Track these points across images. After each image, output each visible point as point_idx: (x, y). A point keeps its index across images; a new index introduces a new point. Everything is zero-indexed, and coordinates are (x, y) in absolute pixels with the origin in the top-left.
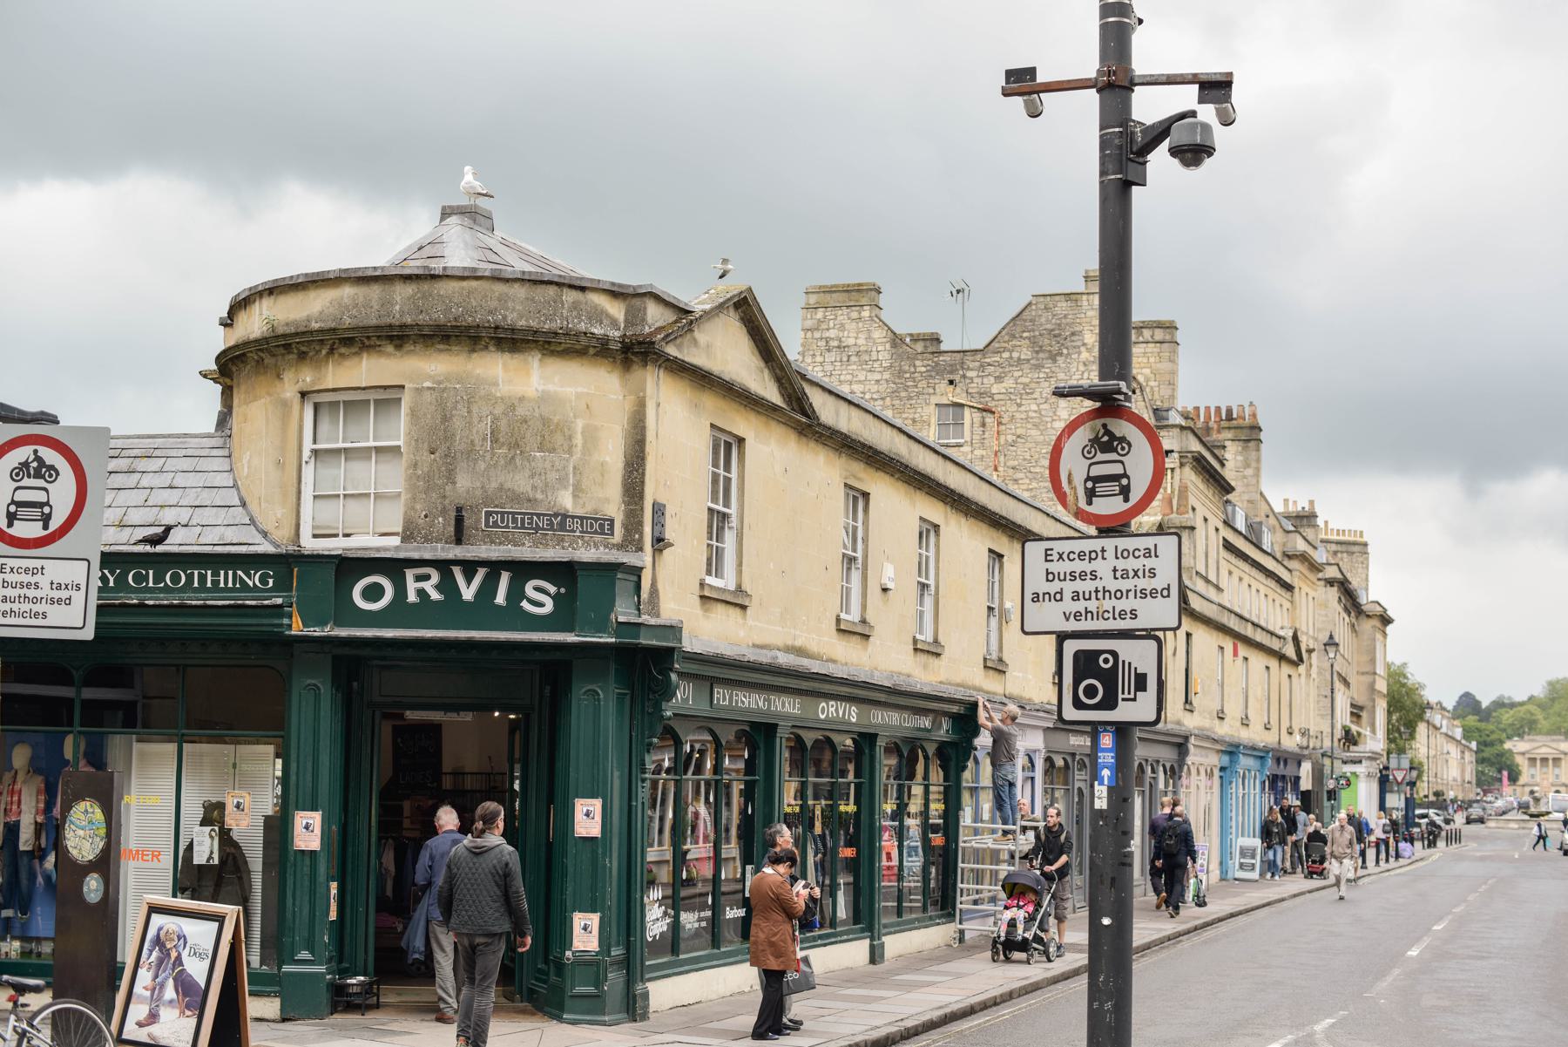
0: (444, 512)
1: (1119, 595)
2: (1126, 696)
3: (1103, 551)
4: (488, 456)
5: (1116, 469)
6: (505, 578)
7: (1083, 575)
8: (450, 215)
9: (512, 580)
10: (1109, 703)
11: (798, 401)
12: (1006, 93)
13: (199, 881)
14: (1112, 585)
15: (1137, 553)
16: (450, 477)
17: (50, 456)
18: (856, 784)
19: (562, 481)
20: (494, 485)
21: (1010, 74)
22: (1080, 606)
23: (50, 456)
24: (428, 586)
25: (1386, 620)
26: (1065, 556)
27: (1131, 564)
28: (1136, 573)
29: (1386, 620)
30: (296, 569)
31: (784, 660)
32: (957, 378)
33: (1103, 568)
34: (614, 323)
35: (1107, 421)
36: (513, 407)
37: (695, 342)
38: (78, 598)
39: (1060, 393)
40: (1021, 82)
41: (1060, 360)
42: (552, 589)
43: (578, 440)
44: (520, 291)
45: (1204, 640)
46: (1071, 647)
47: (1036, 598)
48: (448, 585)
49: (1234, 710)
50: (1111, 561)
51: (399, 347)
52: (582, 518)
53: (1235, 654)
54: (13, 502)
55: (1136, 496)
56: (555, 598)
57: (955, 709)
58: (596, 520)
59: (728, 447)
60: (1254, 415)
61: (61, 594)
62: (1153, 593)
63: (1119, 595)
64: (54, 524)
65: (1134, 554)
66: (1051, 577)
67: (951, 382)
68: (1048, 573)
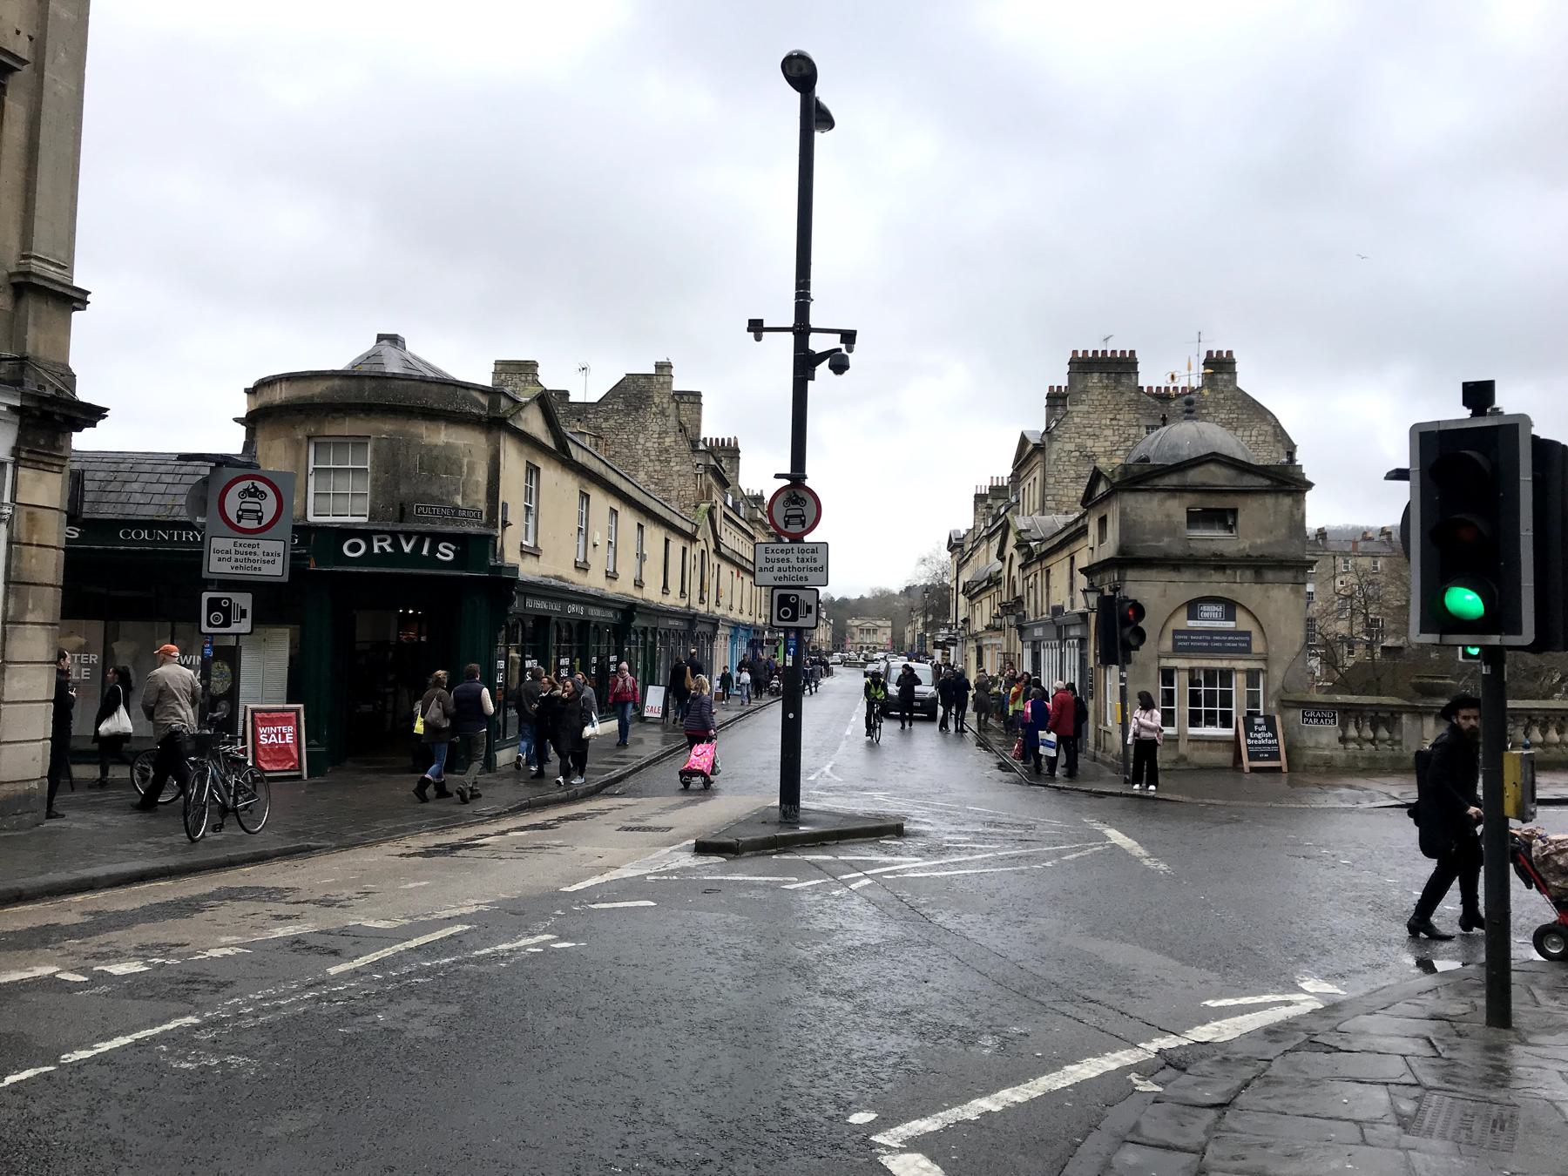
0: (393, 506)
1: (799, 569)
7: (783, 560)
8: (382, 340)
10: (795, 618)
12: (749, 330)
13: (1527, 737)
14: (797, 565)
16: (397, 487)
17: (261, 486)
18: (578, 647)
21: (750, 321)
23: (261, 486)
24: (385, 545)
27: (806, 556)
30: (313, 536)
31: (554, 582)
32: (582, 418)
33: (792, 557)
34: (482, 406)
37: (520, 418)
38: (279, 560)
39: (778, 476)
40: (756, 327)
41: (641, 411)
42: (453, 548)
43: (465, 469)
44: (435, 388)
45: (726, 569)
46: (777, 593)
47: (761, 570)
48: (396, 545)
49: (736, 606)
51: (367, 415)
53: (738, 576)
54: (240, 509)
55: (807, 526)
57: (621, 606)
59: (533, 471)
60: (736, 443)
61: (269, 558)
62: (815, 569)
63: (799, 569)
64: (264, 522)
67: (579, 420)
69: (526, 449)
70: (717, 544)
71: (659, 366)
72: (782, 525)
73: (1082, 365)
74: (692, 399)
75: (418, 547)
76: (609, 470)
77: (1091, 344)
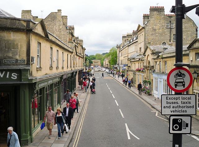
1: (182, 107)
2: (184, 128)
3: (179, 98)
4: (4, 50)
5: (182, 80)
6: (8, 73)
7: (175, 103)
9: (9, 73)
11: (47, 36)
14: (181, 105)
15: (186, 99)
19: (17, 54)
20: (5, 55)
22: (174, 109)
25: (85, 49)
26: (171, 99)
27: (185, 101)
28: (186, 102)
29: (85, 49)
33: (179, 101)
34: (25, 26)
35: (180, 70)
36: (8, 41)
42: (17, 75)
43: (19, 47)
44: (9, 21)
46: (172, 118)
47: (164, 107)
50: (181, 100)
52: (20, 60)
56: (17, 76)
58: (22, 60)
60: (74, 27)
62: (190, 107)
63: (182, 107)
65: (186, 99)
66: (168, 103)
68: (167, 102)
69: (37, 38)
70: (76, 53)
71: (58, 10)
72: (174, 87)
73: (153, 9)
74: (65, 17)
75: (5, 75)
76: (56, 39)
77: (155, 5)
